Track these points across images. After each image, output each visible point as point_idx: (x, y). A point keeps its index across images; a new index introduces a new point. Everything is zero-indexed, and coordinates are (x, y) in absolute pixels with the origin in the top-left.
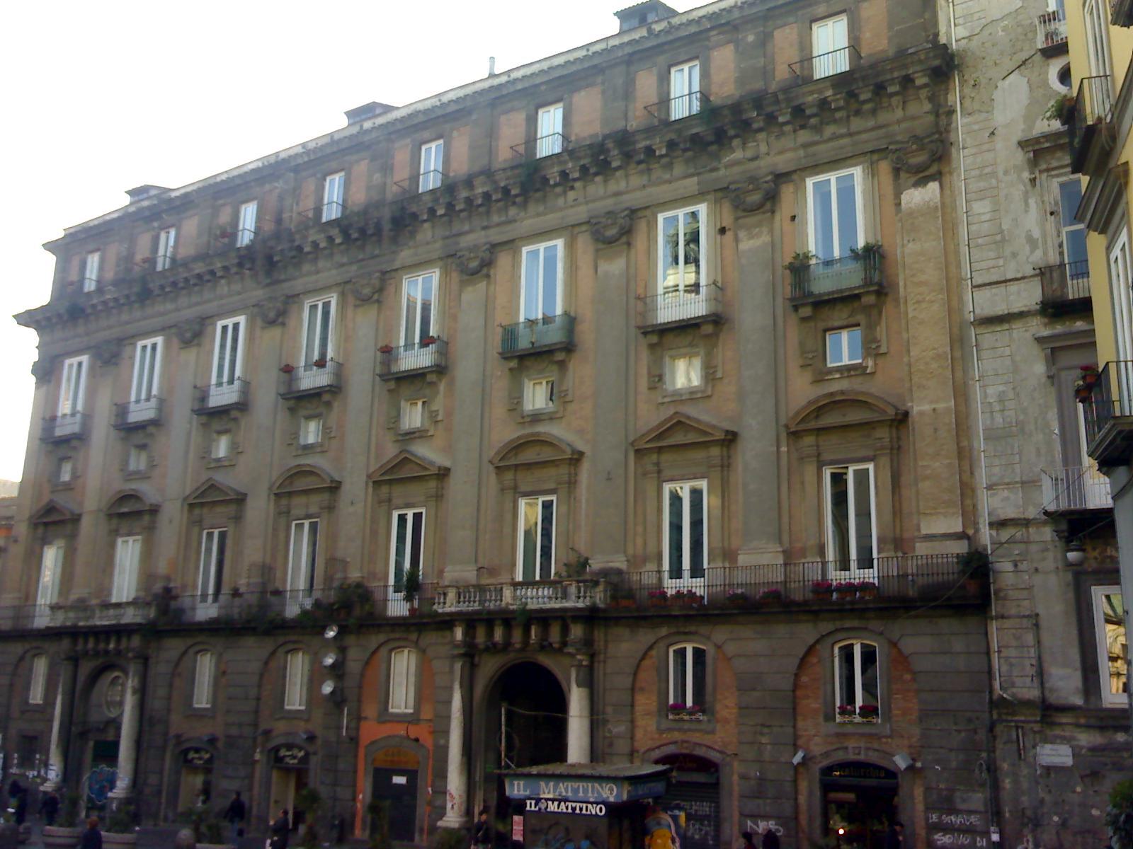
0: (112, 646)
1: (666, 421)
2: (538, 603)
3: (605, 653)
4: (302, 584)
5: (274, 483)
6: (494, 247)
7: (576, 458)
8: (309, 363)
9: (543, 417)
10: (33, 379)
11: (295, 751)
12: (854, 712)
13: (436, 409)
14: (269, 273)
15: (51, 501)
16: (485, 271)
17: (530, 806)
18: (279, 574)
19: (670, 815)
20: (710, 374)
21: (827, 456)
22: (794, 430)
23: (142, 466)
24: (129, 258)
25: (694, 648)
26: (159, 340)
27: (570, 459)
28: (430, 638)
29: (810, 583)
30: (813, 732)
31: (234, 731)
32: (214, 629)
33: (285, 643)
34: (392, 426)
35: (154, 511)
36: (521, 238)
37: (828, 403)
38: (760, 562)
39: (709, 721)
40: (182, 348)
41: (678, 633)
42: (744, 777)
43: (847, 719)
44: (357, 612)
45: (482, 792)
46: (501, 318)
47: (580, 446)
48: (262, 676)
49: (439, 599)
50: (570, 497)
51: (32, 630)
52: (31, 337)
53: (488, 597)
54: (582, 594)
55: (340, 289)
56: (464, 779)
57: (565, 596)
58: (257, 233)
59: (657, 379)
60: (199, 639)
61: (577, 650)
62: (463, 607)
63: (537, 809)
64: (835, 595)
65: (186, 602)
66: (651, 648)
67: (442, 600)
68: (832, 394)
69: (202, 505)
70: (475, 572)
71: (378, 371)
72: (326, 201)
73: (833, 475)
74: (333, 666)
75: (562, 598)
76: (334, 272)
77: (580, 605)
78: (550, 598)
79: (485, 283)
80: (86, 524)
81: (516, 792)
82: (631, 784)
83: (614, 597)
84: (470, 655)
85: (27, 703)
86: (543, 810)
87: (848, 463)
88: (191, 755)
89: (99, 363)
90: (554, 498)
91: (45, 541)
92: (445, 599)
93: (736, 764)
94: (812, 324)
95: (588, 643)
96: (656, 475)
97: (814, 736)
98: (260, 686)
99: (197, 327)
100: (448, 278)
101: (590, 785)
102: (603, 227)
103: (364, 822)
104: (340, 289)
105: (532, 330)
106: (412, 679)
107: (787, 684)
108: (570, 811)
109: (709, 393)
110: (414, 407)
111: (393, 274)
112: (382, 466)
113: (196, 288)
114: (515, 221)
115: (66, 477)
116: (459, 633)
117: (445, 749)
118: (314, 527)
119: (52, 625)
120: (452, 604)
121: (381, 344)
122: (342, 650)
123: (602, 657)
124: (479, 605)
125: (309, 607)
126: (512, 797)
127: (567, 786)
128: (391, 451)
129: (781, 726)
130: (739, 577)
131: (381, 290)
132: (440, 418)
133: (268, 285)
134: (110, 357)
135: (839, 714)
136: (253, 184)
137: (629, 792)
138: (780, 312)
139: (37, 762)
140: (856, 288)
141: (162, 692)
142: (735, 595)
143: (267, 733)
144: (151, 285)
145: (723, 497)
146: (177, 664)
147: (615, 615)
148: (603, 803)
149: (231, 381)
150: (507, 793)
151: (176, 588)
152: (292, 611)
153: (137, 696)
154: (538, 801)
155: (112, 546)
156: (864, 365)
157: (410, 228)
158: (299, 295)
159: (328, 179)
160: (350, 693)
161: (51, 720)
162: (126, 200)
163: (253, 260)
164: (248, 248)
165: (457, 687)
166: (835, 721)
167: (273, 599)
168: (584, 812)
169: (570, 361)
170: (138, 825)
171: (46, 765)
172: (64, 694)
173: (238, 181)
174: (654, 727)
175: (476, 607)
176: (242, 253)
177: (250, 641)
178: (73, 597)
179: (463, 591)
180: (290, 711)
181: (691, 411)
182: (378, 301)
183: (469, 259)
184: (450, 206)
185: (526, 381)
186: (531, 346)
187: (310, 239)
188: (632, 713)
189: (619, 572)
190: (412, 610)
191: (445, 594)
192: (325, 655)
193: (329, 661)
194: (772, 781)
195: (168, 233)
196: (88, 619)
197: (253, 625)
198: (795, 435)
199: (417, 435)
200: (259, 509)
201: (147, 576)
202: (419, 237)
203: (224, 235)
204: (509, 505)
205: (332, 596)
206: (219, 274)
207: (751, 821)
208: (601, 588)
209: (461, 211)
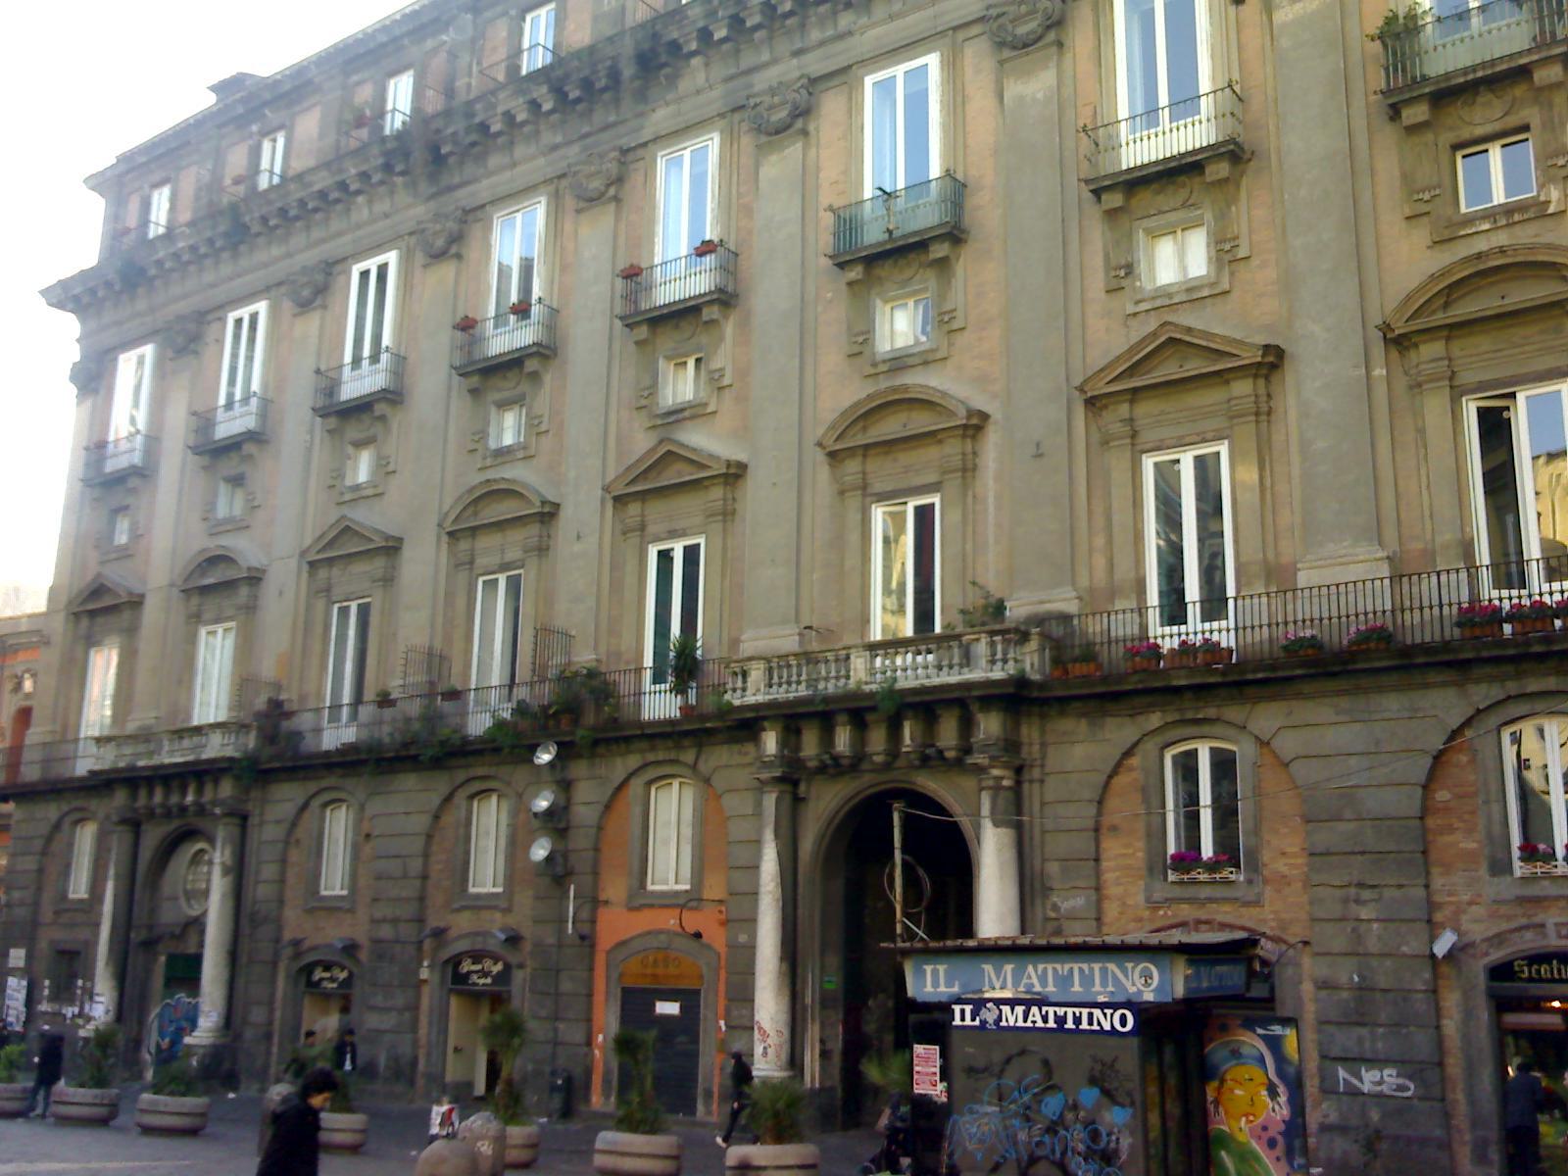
0: (190, 798)
1: (1143, 341)
2: (917, 678)
3: (1042, 766)
4: (497, 676)
5: (447, 514)
6: (814, 83)
7: (975, 425)
8: (502, 311)
9: (910, 361)
10: (73, 390)
11: (488, 964)
12: (1553, 856)
13: (719, 366)
14: (433, 177)
15: (99, 575)
16: (799, 124)
17: (962, 1017)
18: (456, 669)
19: (1264, 1038)
20: (1225, 253)
21: (1467, 377)
22: (1402, 331)
23: (238, 509)
24: (215, 185)
25: (1212, 749)
26: (262, 307)
27: (965, 427)
28: (720, 757)
29: (1455, 608)
30: (1466, 898)
31: (386, 932)
32: (351, 762)
33: (469, 780)
34: (644, 402)
35: (255, 579)
36: (862, 62)
37: (1470, 276)
38: (1342, 579)
39: (1250, 882)
40: (295, 316)
41: (1184, 722)
42: (1323, 985)
43: (1539, 868)
44: (590, 718)
45: (817, 1027)
46: (827, 197)
47: (980, 402)
48: (429, 837)
49: (734, 683)
50: (965, 495)
51: (71, 780)
52: (68, 326)
53: (823, 673)
54: (999, 656)
55: (551, 188)
56: (785, 1001)
57: (967, 660)
58: (416, 110)
59: (1122, 273)
60: (325, 783)
61: (992, 758)
62: (780, 694)
63: (977, 1023)
64: (1507, 628)
65: (304, 721)
66: (1128, 753)
67: (739, 684)
68: (1479, 256)
69: (330, 561)
70: (797, 638)
71: (618, 310)
72: (526, 44)
73: (1483, 413)
74: (549, 813)
75: (961, 666)
76: (541, 161)
77: (997, 674)
78: (940, 668)
79: (799, 145)
80: (152, 614)
81: (929, 988)
82: (1191, 962)
83: (1057, 661)
84: (792, 779)
85: (64, 897)
86: (991, 1025)
87: (1512, 386)
88: (319, 974)
89: (170, 353)
90: (935, 499)
91: (91, 641)
92: (745, 681)
93: (1307, 961)
94: (1429, 137)
95: (1011, 746)
96: (1128, 441)
97: (1471, 903)
98: (426, 855)
99: (319, 278)
100: (735, 146)
101: (1097, 967)
102: (1011, 22)
103: (606, 1082)
104: (551, 188)
105: (888, 209)
106: (687, 831)
107: (1407, 802)
108: (1051, 1024)
109: (1226, 287)
110: (681, 372)
111: (640, 152)
112: (629, 469)
113: (318, 216)
114: (850, 33)
115: (122, 538)
116: (770, 742)
117: (751, 949)
118: (514, 586)
119: (97, 768)
120: (758, 690)
121: (621, 265)
122: (565, 786)
123: (1036, 773)
124: (807, 688)
125: (507, 715)
126: (919, 1000)
127: (1045, 970)
128: (642, 443)
129: (1400, 886)
130: (1303, 608)
131: (620, 180)
132: (726, 381)
133: (433, 197)
134: (186, 341)
135: (1522, 859)
136: (406, 41)
137: (1187, 978)
138: (1360, 123)
139: (79, 992)
140: (1520, 53)
141: (269, 871)
142: (1300, 641)
143: (439, 934)
144: (247, 219)
145: (1261, 469)
146: (294, 825)
147: (1060, 693)
148: (1128, 1005)
149: (375, 358)
150: (910, 993)
151: (290, 700)
152: (478, 724)
153: (229, 879)
154: (979, 1004)
155: (192, 640)
156: (1542, 198)
157: (667, 70)
158: (483, 206)
159: (529, 18)
160: (575, 863)
161: (97, 925)
162: (211, 99)
163: (406, 155)
164: (400, 136)
165: (769, 836)
166: (1510, 871)
167: (447, 707)
168: (1084, 1026)
169: (958, 259)
170: (235, 1089)
171: (90, 995)
172: (117, 877)
173: (383, 38)
174: (1141, 898)
175: (802, 691)
176: (390, 145)
177: (409, 781)
178: (131, 727)
179: (776, 665)
180: (478, 896)
181: (1188, 318)
182: (617, 199)
183: (771, 108)
184: (737, 22)
185: (879, 303)
186: (887, 235)
187: (500, 109)
188: (1098, 874)
189: (1065, 618)
190: (685, 709)
191: (745, 674)
192: (536, 796)
193: (542, 804)
194: (1384, 991)
195: (274, 141)
196: (151, 754)
197: (413, 752)
198: (1398, 342)
199: (686, 414)
200: (423, 562)
201: (244, 683)
202: (685, 85)
203: (360, 122)
204: (854, 517)
205: (546, 693)
206: (353, 187)
207: (1346, 1070)
208: (1033, 644)
209: (757, 28)
